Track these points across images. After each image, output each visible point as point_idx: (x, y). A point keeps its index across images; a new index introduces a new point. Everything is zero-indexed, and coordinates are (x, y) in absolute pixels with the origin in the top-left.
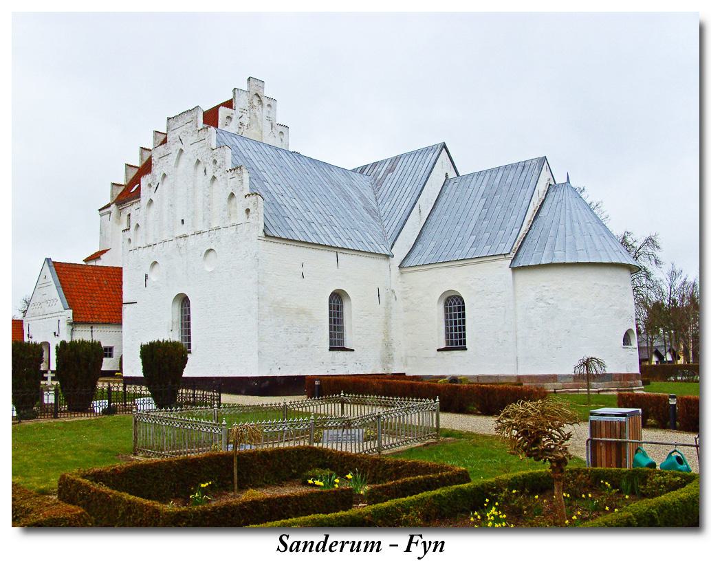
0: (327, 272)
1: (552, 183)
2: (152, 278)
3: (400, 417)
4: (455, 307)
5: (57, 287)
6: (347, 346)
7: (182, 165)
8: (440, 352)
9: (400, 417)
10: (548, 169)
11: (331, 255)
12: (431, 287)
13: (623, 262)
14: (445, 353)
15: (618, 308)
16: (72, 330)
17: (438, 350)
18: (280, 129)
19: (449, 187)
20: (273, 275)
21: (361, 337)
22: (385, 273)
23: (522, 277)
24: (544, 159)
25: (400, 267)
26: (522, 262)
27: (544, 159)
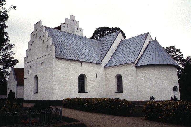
0: (78, 69)
1: (151, 40)
2: (30, 71)
3: (59, 112)
4: (119, 78)
5: (14, 75)
6: (85, 91)
7: (37, 38)
8: (116, 93)
9: (59, 112)
10: (150, 36)
11: (80, 64)
12: (113, 73)
13: (169, 64)
14: (117, 94)
15: (170, 79)
16: (17, 87)
17: (115, 93)
18: (80, 30)
19: (122, 43)
20: (144, 79)
21: (90, 88)
22: (100, 70)
23: (138, 69)
24: (149, 33)
25: (105, 67)
26: (139, 65)
27: (149, 33)
